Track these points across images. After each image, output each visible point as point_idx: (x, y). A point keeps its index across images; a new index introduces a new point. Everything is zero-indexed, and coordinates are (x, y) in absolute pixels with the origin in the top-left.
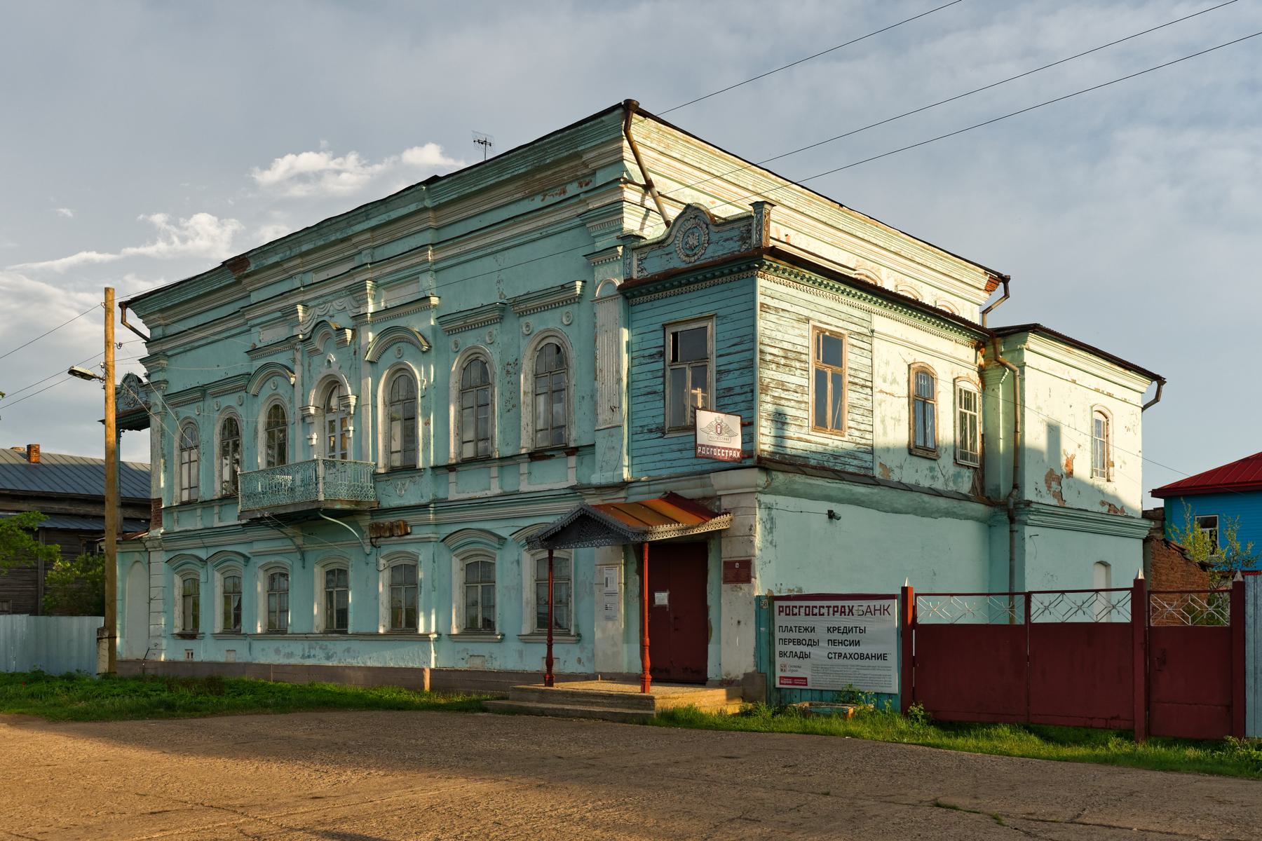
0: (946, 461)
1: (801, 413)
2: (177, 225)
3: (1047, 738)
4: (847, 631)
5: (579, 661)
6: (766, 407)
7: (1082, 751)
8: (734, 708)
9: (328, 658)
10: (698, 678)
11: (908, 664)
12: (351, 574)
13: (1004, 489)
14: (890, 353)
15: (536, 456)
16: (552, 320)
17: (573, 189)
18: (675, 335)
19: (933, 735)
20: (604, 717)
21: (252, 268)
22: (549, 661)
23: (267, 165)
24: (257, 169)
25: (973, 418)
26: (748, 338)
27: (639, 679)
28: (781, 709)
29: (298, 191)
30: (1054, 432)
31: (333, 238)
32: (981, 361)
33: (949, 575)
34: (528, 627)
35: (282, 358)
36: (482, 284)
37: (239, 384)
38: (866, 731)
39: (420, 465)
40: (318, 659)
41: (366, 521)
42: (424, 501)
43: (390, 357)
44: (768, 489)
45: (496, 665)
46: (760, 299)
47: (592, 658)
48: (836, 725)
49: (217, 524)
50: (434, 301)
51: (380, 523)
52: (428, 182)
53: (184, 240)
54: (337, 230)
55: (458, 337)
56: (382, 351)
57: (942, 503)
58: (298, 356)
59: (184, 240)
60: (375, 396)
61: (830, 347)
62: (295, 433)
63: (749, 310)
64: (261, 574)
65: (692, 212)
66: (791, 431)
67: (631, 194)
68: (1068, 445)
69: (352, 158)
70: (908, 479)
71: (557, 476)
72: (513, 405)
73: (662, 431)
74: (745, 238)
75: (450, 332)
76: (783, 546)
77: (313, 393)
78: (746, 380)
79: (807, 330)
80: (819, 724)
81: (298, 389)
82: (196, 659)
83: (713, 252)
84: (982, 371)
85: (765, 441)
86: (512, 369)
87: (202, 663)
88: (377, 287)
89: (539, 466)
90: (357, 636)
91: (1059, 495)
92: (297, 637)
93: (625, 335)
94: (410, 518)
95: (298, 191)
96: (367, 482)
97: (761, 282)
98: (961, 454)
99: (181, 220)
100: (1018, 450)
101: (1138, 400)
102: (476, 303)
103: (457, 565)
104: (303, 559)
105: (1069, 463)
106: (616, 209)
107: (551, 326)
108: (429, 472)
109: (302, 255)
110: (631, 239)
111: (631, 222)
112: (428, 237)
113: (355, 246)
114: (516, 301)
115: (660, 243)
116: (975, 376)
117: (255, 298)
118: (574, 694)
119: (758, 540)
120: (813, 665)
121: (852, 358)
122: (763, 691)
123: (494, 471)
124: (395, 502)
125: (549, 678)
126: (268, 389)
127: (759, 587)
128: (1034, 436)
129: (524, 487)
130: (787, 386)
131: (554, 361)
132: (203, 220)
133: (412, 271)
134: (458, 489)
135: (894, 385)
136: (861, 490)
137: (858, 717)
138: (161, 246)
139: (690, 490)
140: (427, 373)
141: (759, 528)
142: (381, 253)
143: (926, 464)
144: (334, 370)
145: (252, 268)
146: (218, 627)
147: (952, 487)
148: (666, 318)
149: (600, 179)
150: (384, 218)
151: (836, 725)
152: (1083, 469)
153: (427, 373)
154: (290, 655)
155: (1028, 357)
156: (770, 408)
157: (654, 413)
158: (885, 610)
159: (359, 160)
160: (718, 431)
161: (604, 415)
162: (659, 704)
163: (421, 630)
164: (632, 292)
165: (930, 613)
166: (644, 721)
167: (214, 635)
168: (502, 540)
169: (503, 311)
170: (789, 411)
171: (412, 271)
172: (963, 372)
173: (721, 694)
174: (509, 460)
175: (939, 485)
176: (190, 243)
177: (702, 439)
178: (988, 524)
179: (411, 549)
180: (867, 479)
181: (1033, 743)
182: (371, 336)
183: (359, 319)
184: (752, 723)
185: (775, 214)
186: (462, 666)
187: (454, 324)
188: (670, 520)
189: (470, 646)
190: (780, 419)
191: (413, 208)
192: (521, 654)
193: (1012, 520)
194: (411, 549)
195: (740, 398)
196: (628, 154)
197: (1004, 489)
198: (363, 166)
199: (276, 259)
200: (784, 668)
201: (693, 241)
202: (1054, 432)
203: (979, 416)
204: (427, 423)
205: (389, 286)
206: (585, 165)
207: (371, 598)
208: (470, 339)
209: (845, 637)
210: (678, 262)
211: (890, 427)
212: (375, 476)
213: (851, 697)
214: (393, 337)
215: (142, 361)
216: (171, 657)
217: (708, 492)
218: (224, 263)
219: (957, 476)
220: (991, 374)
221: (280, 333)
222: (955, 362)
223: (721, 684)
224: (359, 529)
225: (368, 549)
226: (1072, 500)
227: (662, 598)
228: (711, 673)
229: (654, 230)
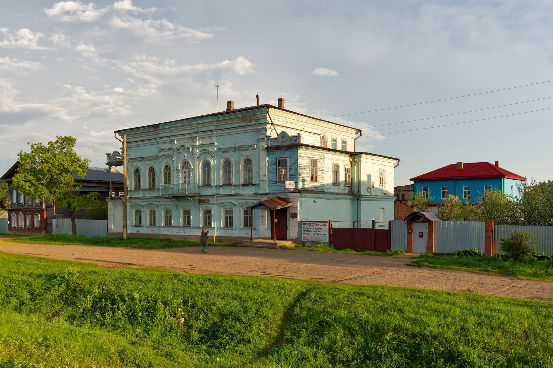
0: (342, 186)
1: (308, 179)
2: (13, 34)
3: (357, 251)
6: (301, 178)
7: (361, 253)
8: (293, 245)
10: (284, 239)
11: (330, 236)
12: (192, 212)
13: (356, 192)
14: (328, 160)
15: (243, 185)
16: (248, 153)
17: (253, 122)
19: (335, 250)
20: (266, 247)
21: (160, 128)
22: (251, 235)
23: (51, 6)
24: (46, 8)
25: (349, 175)
26: (296, 163)
27: (272, 238)
28: (304, 246)
29: (66, 19)
30: (369, 177)
32: (351, 160)
33: (341, 215)
34: (242, 226)
35: (170, 153)
36: (229, 141)
37: (156, 158)
38: (321, 250)
39: (212, 185)
40: (181, 233)
41: (197, 198)
42: (213, 194)
43: (203, 157)
44: (301, 197)
45: (233, 235)
46: (299, 155)
47: (259, 233)
48: (315, 248)
49: (147, 196)
50: (216, 144)
51: (201, 199)
53: (16, 40)
55: (223, 154)
56: (201, 155)
57: (341, 196)
58: (175, 153)
59: (16, 40)
60: (199, 166)
61: (314, 163)
62: (173, 174)
63: (297, 157)
64: (163, 210)
65: (283, 133)
66: (306, 183)
67: (268, 126)
68: (373, 180)
69: (91, 5)
70: (332, 191)
71: (250, 190)
72: (238, 172)
73: (276, 182)
74: (296, 141)
75: (220, 152)
76: (304, 209)
77: (180, 164)
79: (309, 160)
80: (312, 248)
81: (175, 162)
82: (140, 232)
83: (288, 143)
84: (351, 163)
85: (300, 186)
86: (238, 163)
87: (143, 234)
88: (199, 138)
89: (245, 188)
90: (194, 227)
91: (370, 192)
92: (174, 227)
93: (267, 159)
94: (209, 198)
95: (66, 19)
96: (197, 188)
97: (299, 151)
98: (346, 183)
99: (14, 31)
100: (359, 182)
101: (393, 165)
102: (227, 146)
103: (222, 210)
104: (176, 207)
105: (373, 184)
106: (265, 129)
107: (248, 154)
109: (176, 127)
110: (268, 137)
111: (268, 133)
112: (214, 128)
114: (239, 147)
115: (276, 139)
116: (350, 164)
117: (160, 135)
118: (258, 242)
119: (299, 208)
120: (310, 236)
121: (319, 165)
122: (300, 242)
123: (233, 188)
124: (205, 194)
125: (251, 239)
126: (165, 161)
127: (299, 219)
128: (364, 178)
129: (241, 192)
130: (306, 174)
131: (248, 162)
132: (25, 32)
134: (222, 191)
135: (329, 169)
136: (321, 195)
137: (320, 247)
138: (6, 42)
139: (283, 196)
140: (214, 162)
141: (299, 206)
142: (200, 130)
143: (337, 187)
144: (186, 158)
146: (148, 224)
147: (343, 192)
149: (261, 122)
150: (202, 121)
151: (315, 248)
152: (377, 185)
153: (214, 162)
154: (173, 232)
155: (362, 160)
156: (301, 179)
157: (274, 178)
158: (326, 225)
159: (94, 6)
160: (290, 185)
161: (262, 177)
162: (278, 245)
163: (213, 226)
164: (268, 149)
165: (335, 225)
166: (275, 248)
167: (147, 226)
168: (235, 205)
169: (235, 149)
170: (306, 179)
172: (346, 163)
173: (290, 242)
174: (236, 186)
175: (340, 192)
176: (19, 42)
177: (287, 187)
178: (352, 200)
179: (209, 206)
180: (323, 192)
181: (354, 252)
182: (197, 151)
183: (194, 147)
184: (298, 248)
185: (302, 136)
186: (224, 235)
187: (221, 151)
188: (281, 205)
190: (303, 181)
191: (210, 120)
192: (240, 232)
193: (358, 199)
194: (209, 206)
195: (295, 177)
196: (268, 116)
197: (356, 192)
198: (95, 9)
200: (305, 236)
201: (284, 140)
202: (369, 177)
203: (350, 174)
204: (214, 175)
205: (203, 138)
207: (197, 218)
208: (226, 155)
209: (317, 230)
210: (280, 144)
211: (326, 178)
212: (199, 187)
213: (318, 243)
214: (204, 152)
215: (121, 148)
216: (132, 232)
217: (287, 197)
219: (344, 189)
220: (353, 163)
221: (168, 146)
222: (344, 161)
223: (290, 240)
224: (194, 200)
225: (197, 205)
226: (374, 193)
228: (288, 237)
229: (274, 136)
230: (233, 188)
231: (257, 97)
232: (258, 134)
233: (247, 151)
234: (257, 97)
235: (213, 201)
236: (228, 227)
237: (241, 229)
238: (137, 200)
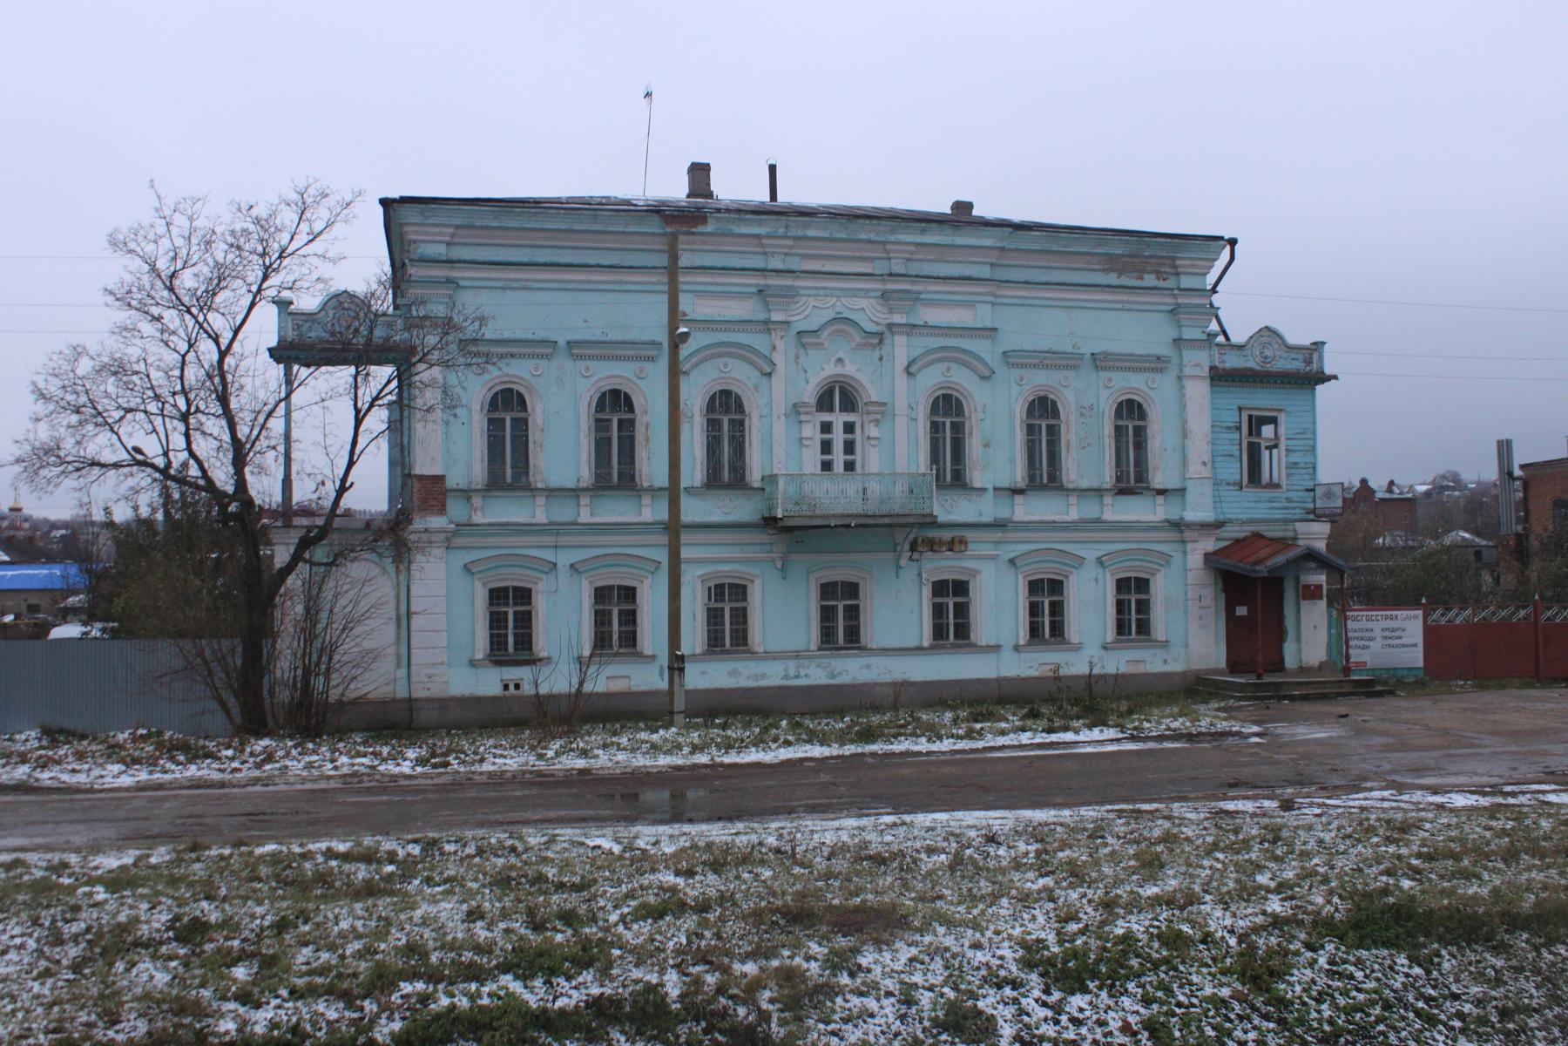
4: (1394, 630)
5: (1165, 662)
9: (833, 676)
18: (1250, 417)
21: (709, 228)
74: (1309, 362)
78: (1309, 459)
83: (1283, 364)
94: (969, 535)
108: (991, 491)
112: (985, 272)
148: (1241, 403)
189: (1037, 655)
206: (1175, 267)
227: (1242, 611)
230: (541, 501)
231: (773, 169)
232: (767, 304)
233: (1130, 375)
234: (773, 169)
235: (980, 545)
236: (1044, 642)
237: (1017, 648)
238: (523, 540)
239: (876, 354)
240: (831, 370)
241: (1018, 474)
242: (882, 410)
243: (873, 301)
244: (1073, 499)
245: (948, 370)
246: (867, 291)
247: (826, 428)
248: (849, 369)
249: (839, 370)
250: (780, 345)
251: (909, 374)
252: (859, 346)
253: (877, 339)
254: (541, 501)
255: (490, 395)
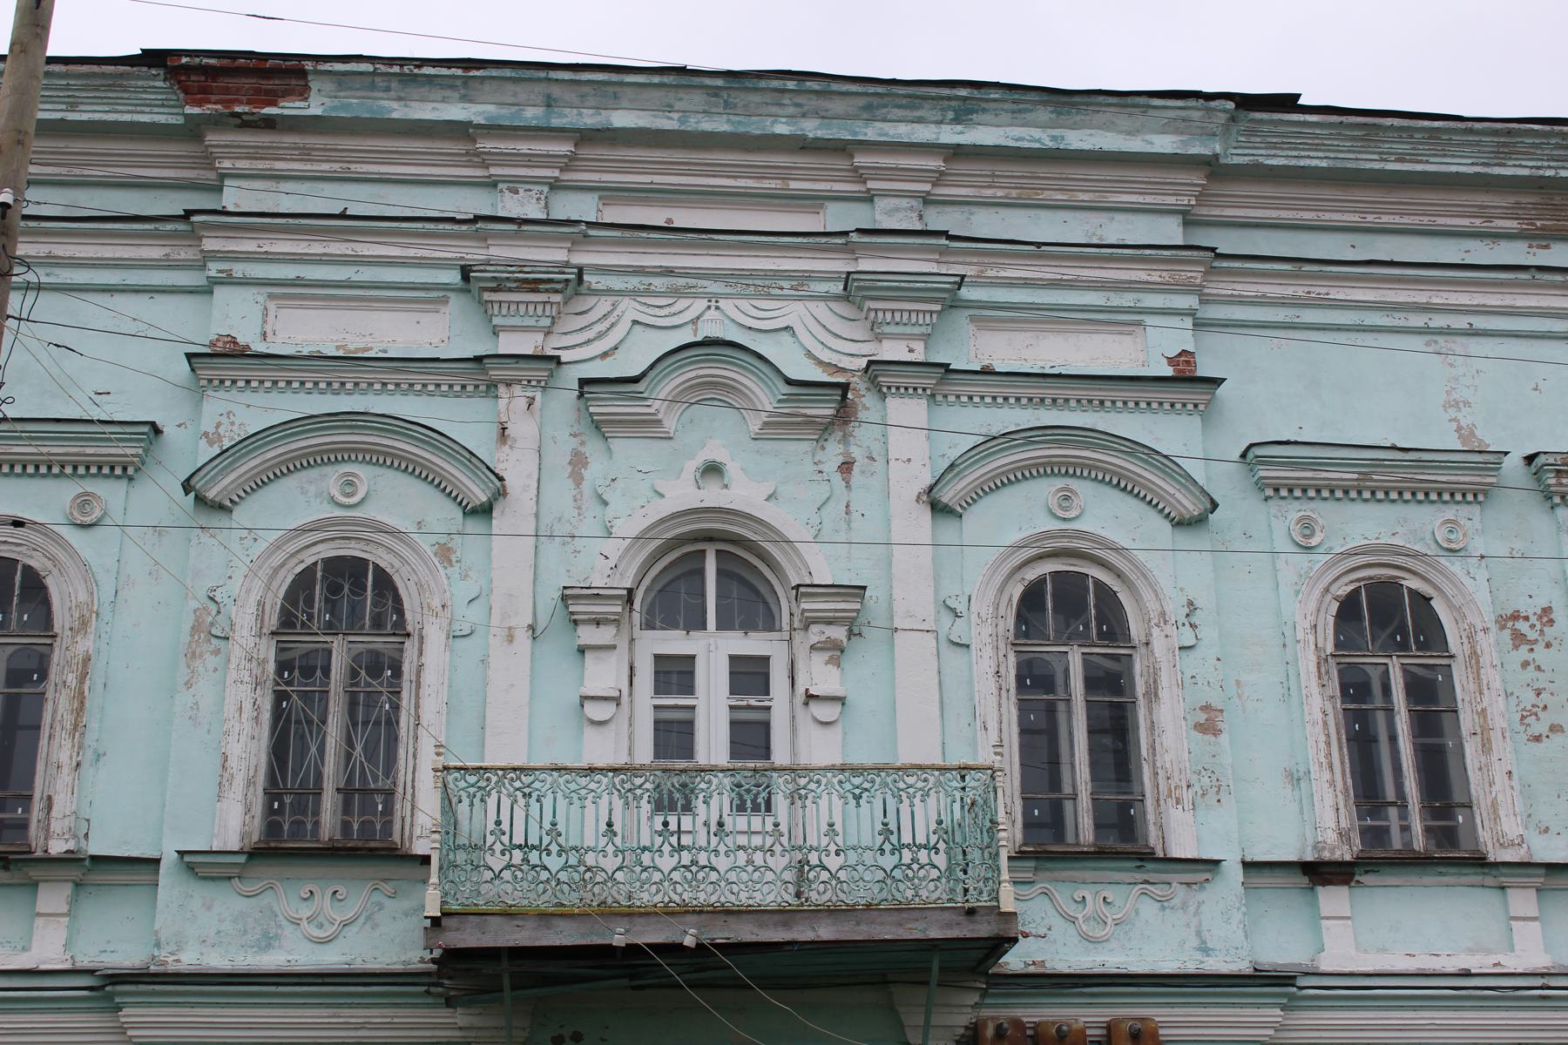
31: (782, 129)
52: (1247, 102)
54: (817, 114)
108: (1233, 873)
113: (859, 175)
117: (234, 197)
133: (1127, 300)
145: (315, 106)
171: (1127, 300)
199: (455, 112)
218: (152, 58)
239: (833, 453)
240: (684, 493)
241: (1322, 820)
242: (847, 613)
243: (820, 309)
244: (1522, 901)
245: (1067, 497)
246: (808, 276)
247: (675, 674)
248: (742, 492)
249: (712, 496)
250: (523, 428)
251: (939, 509)
252: (778, 427)
253: (827, 406)
254: (53, 898)
255: (1017, 591)
